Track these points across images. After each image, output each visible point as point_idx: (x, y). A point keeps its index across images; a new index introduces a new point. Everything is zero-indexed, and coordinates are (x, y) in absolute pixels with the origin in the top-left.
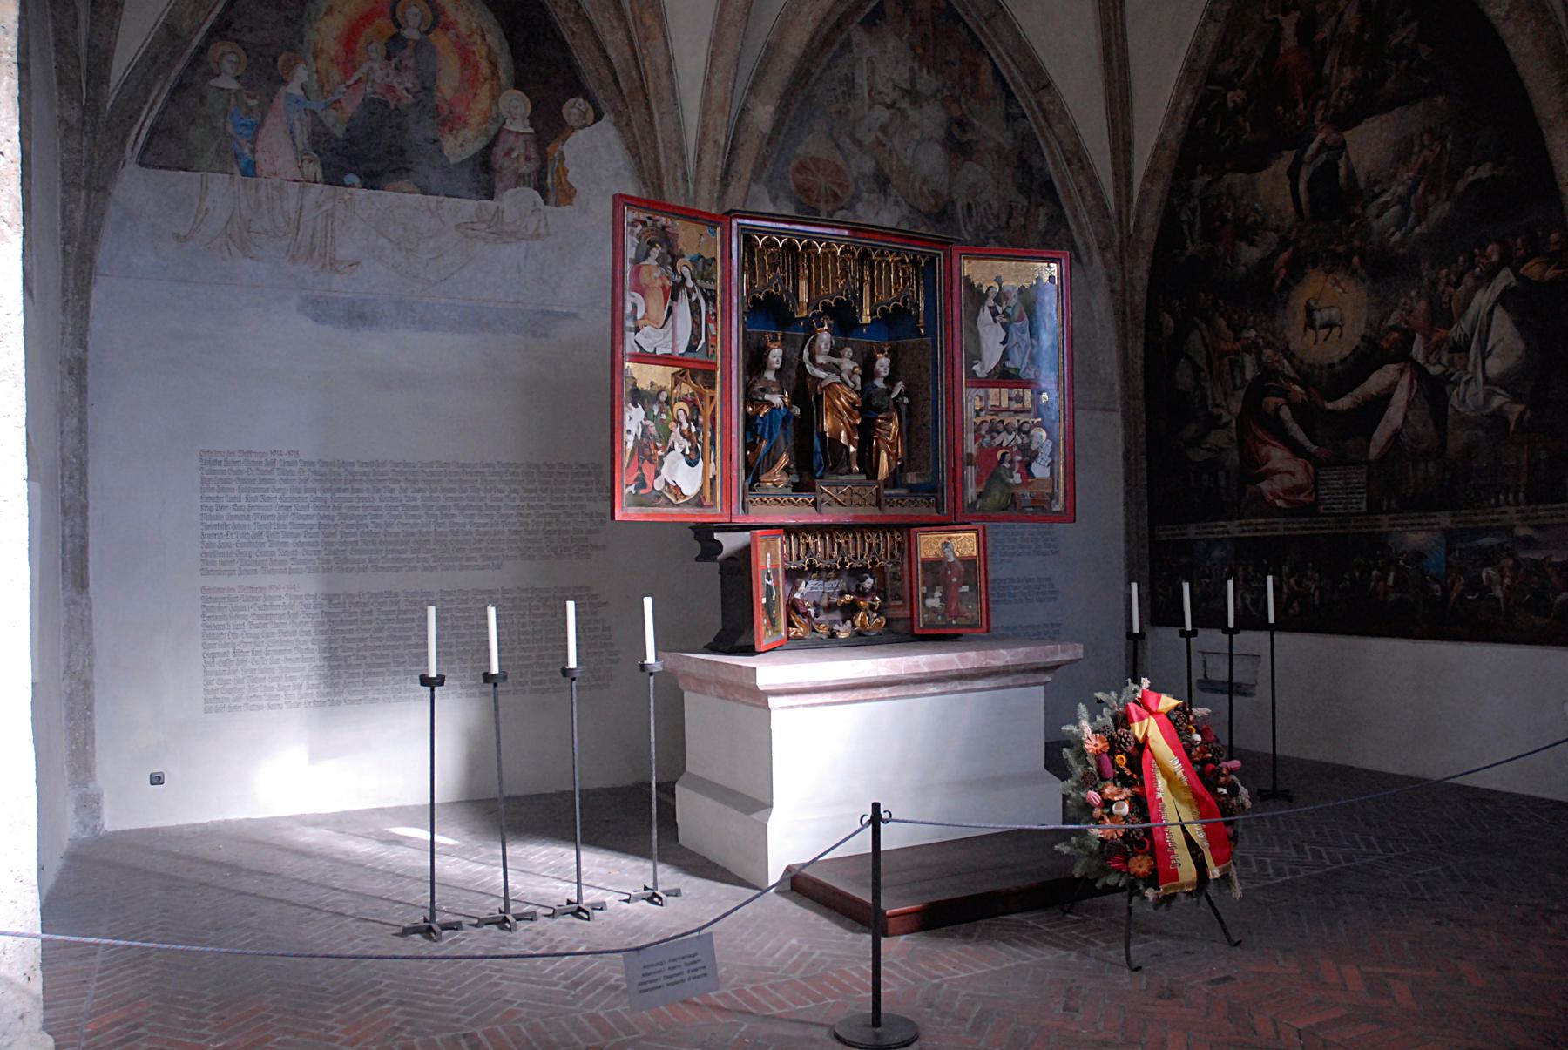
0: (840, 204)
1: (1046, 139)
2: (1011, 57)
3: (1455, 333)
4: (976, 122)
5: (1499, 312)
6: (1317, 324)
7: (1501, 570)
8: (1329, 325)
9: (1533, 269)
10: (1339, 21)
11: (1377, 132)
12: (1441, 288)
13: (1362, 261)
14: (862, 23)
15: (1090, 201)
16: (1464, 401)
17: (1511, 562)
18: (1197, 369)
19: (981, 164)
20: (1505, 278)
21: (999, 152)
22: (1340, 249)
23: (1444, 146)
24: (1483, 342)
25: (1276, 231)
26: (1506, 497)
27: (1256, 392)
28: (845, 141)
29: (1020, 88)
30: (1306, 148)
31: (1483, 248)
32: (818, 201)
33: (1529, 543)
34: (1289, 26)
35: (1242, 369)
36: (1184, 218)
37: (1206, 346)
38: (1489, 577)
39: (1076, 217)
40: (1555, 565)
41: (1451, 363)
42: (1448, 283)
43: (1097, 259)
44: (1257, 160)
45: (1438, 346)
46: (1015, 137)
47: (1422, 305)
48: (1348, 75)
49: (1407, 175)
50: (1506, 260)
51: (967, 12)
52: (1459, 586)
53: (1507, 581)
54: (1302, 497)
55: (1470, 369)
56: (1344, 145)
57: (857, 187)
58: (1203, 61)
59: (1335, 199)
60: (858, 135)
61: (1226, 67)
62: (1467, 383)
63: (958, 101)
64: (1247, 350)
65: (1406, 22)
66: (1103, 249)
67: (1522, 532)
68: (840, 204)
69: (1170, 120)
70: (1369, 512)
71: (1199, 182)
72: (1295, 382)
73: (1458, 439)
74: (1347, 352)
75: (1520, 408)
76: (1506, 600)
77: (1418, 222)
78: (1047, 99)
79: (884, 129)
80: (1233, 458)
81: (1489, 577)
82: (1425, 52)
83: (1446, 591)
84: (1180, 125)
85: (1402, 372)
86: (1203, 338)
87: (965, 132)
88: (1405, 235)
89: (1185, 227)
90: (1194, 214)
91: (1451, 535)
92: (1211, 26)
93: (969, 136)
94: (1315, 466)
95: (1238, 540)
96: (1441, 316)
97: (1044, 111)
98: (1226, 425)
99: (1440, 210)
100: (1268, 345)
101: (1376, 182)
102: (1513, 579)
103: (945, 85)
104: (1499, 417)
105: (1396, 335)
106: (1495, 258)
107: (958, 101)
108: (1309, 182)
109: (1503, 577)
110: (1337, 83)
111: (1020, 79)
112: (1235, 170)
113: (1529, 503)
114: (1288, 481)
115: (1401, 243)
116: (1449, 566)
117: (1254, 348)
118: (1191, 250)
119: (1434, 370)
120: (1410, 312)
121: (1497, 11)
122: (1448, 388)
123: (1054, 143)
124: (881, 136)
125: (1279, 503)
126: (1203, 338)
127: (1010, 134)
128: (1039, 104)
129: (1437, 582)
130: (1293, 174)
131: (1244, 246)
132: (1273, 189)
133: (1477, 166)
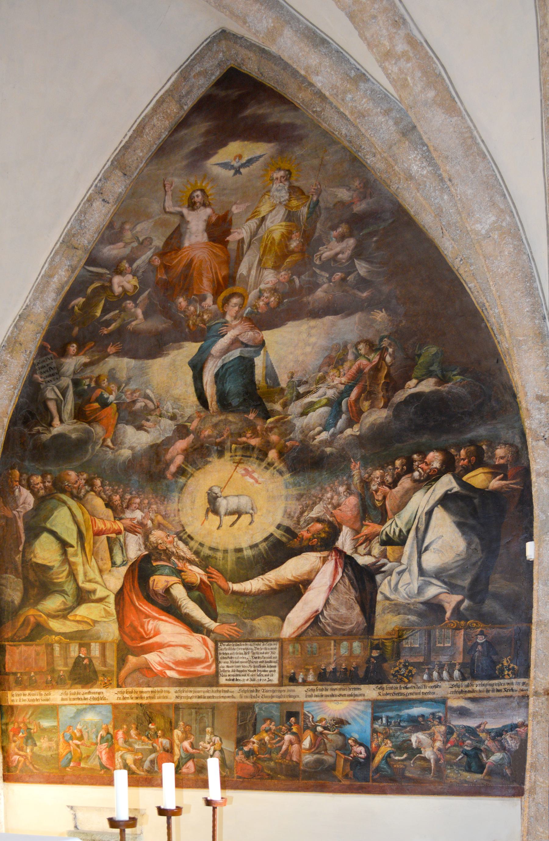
3: (390, 528)
5: (439, 514)
6: (222, 511)
7: (432, 737)
8: (238, 513)
9: (478, 478)
10: (259, 227)
11: (304, 336)
12: (374, 487)
13: (281, 454)
16: (396, 589)
17: (443, 728)
18: (64, 545)
20: (447, 483)
22: (254, 442)
23: (382, 358)
24: (420, 541)
25: (173, 418)
26: (440, 674)
27: (141, 572)
30: (215, 342)
31: (423, 454)
33: (463, 712)
34: (197, 223)
35: (124, 548)
36: (50, 394)
37: (76, 522)
38: (419, 742)
40: (489, 732)
41: (384, 555)
42: (383, 483)
44: (155, 346)
45: (369, 539)
47: (353, 500)
48: (270, 277)
49: (338, 380)
50: (449, 466)
52: (386, 748)
53: (438, 744)
54: (199, 669)
55: (404, 560)
56: (262, 344)
58: (87, 240)
59: (246, 394)
61: (111, 251)
62: (400, 573)
64: (131, 530)
65: (342, 238)
67: (455, 703)
69: (40, 290)
70: (281, 684)
71: (71, 363)
72: (191, 562)
73: (386, 624)
74: (258, 538)
75: (459, 598)
76: (437, 761)
77: (350, 424)
80: (110, 631)
81: (419, 742)
82: (362, 268)
83: (371, 756)
84: (51, 301)
85: (325, 560)
86: (73, 516)
88: (334, 435)
89: (52, 406)
90: (64, 392)
91: (377, 706)
92: (97, 204)
94: (216, 642)
95: (115, 706)
96: (372, 510)
98: (101, 600)
99: (376, 416)
100: (159, 526)
101: (301, 383)
102: (445, 742)
104: (434, 608)
105: (319, 526)
106: (436, 465)
108: (217, 376)
109: (434, 741)
110: (257, 284)
112: (118, 354)
113: (464, 679)
114: (181, 654)
115: (329, 443)
116: (374, 731)
117: (141, 529)
118: (58, 428)
119: (363, 560)
120: (337, 506)
121: (478, 227)
122: (378, 578)
125: (170, 673)
126: (73, 516)
129: (361, 745)
130: (197, 367)
131: (130, 430)
132: (170, 378)
133: (420, 381)
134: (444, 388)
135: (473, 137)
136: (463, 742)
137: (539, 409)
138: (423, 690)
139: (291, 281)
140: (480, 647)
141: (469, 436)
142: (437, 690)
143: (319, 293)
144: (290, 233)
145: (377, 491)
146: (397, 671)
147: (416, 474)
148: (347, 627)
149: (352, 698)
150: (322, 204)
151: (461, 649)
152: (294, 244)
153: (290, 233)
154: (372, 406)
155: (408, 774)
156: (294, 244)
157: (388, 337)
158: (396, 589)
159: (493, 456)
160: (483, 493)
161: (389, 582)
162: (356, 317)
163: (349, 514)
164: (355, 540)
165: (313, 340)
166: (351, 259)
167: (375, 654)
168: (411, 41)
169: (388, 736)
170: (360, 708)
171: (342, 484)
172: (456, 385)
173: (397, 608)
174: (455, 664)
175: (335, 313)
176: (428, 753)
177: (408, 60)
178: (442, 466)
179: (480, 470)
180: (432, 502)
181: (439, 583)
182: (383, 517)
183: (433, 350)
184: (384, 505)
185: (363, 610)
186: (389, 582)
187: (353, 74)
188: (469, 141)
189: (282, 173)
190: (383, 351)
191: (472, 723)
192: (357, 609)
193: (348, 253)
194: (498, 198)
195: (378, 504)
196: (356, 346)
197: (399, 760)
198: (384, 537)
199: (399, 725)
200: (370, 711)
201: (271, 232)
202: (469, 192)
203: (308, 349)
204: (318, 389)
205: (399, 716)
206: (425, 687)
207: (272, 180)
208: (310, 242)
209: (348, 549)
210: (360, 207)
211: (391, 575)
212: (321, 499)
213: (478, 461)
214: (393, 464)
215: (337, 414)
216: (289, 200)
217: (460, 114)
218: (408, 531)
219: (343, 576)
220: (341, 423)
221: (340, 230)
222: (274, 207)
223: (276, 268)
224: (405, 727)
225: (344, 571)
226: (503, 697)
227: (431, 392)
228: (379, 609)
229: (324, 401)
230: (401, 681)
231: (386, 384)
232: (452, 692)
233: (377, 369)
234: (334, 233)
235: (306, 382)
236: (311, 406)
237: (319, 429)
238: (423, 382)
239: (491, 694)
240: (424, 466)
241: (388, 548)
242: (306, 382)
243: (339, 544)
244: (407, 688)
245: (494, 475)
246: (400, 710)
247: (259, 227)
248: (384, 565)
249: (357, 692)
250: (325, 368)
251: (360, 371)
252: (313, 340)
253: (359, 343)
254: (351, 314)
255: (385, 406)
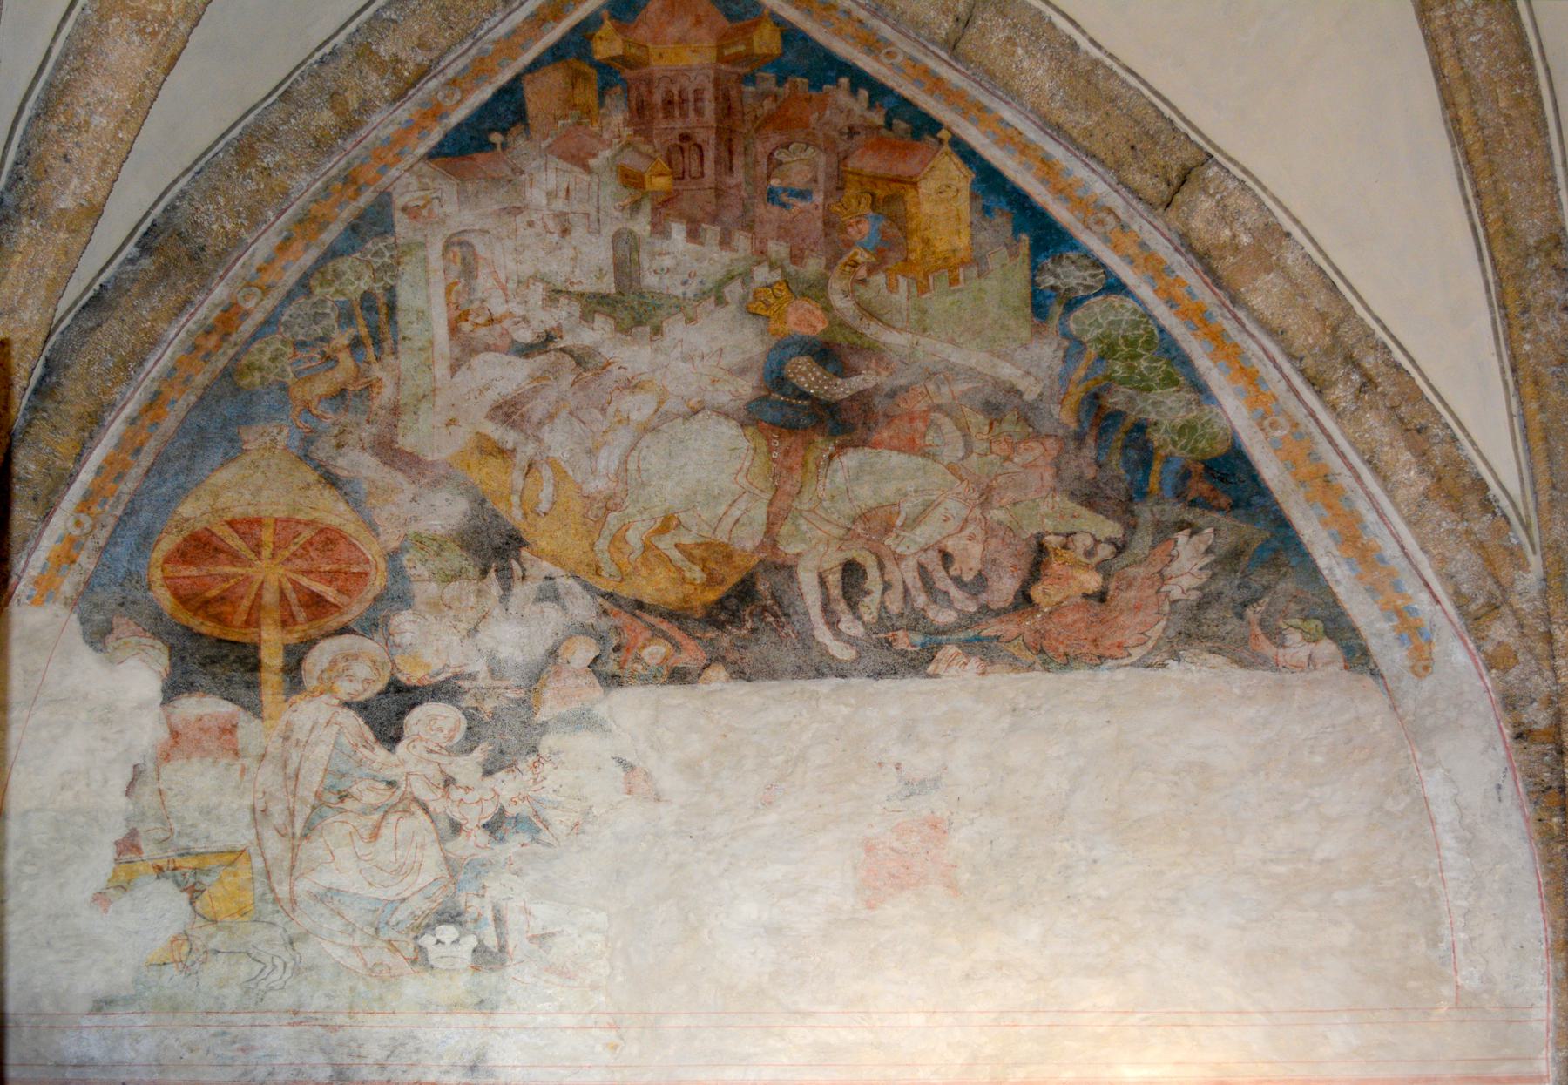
0: (334, 622)
1: (1217, 338)
2: (1056, 130)
4: (895, 339)
14: (431, 156)
15: (1412, 479)
19: (911, 447)
21: (999, 406)
28: (359, 464)
29: (1093, 211)
32: (252, 622)
39: (1351, 538)
43: (1456, 655)
46: (1074, 346)
51: (873, 45)
57: (397, 572)
60: (406, 442)
63: (816, 290)
66: (1474, 620)
68: (334, 622)
78: (1200, 212)
79: (508, 411)
87: (845, 371)
93: (856, 383)
97: (1204, 259)
103: (761, 255)
107: (816, 290)
111: (1100, 188)
123: (1256, 347)
124: (494, 431)
127: (1047, 352)
128: (1186, 244)
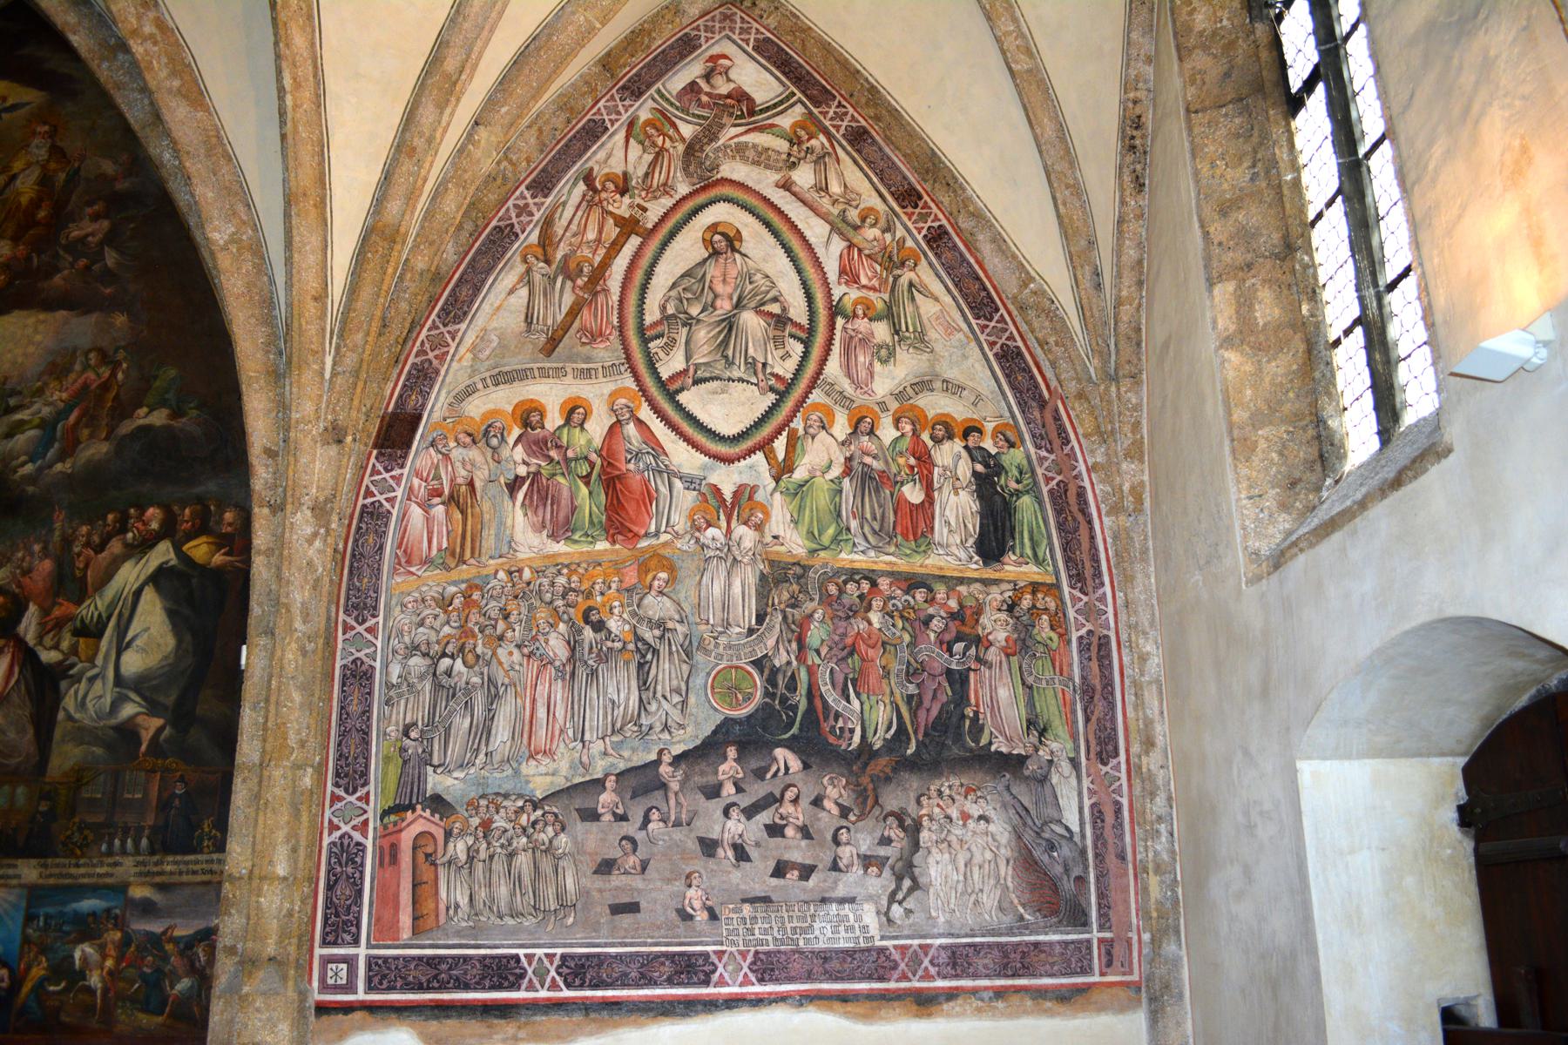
3: (89, 610)
5: (149, 595)
7: (102, 949)
9: (199, 549)
11: (29, 331)
20: (164, 553)
23: (113, 375)
24: (122, 630)
26: (123, 843)
31: (142, 509)
33: (147, 909)
38: (84, 959)
41: (74, 650)
42: (88, 544)
47: (47, 565)
50: (169, 530)
55: (99, 661)
62: (92, 680)
65: (95, 218)
67: (138, 892)
73: (65, 757)
76: (105, 991)
77: (61, 458)
82: (111, 258)
88: (40, 470)
99: (95, 450)
101: (14, 393)
102: (118, 960)
104: (128, 732)
106: (154, 525)
109: (104, 957)
113: (152, 853)
115: (32, 479)
116: (26, 940)
119: (48, 656)
122: (63, 684)
134: (179, 424)
135: (218, 137)
136: (143, 959)
137: (267, 466)
138: (99, 870)
139: (28, 259)
140: (177, 802)
141: (198, 490)
142: (119, 869)
143: (57, 279)
144: (41, 200)
145: (79, 555)
146: (69, 837)
147: (130, 535)
148: (14, 761)
149: (1023, 813)
150: (82, 173)
151: (154, 803)
152: (42, 214)
153: (41, 200)
154: (91, 436)
155: (65, 1018)
156: (42, 214)
157: (124, 348)
158: (82, 705)
159: (220, 521)
160: (203, 570)
161: (76, 693)
162: (93, 318)
163: (41, 584)
164: (41, 624)
165: (38, 338)
166: (101, 244)
167: (43, 807)
168: (160, 24)
169: (44, 950)
170: (12, 898)
171: (37, 541)
172: (189, 423)
173: (82, 734)
174: (143, 828)
175: (70, 308)
176: (95, 980)
177: (155, 43)
178: (161, 526)
179: (203, 539)
180: (142, 578)
181: (138, 699)
182: (81, 595)
183: (172, 373)
184: (85, 575)
185: (37, 733)
186: (76, 693)
187: (113, 41)
188: (214, 140)
189: (46, 128)
190: (116, 365)
191: (156, 927)
192: (31, 732)
193: (99, 236)
194: (240, 208)
195: (78, 574)
196: (86, 354)
197: (54, 993)
198: (78, 624)
199: (60, 930)
200: (24, 904)
201: (19, 194)
202: (210, 194)
203: (31, 349)
204: (32, 403)
205: (62, 914)
206: (102, 864)
207: (34, 134)
208: (61, 216)
209: (30, 638)
210: (122, 185)
211: (79, 681)
212: (9, 560)
213: (201, 529)
214: (105, 518)
215: (47, 442)
216: (48, 161)
217: (208, 110)
218: (109, 618)
219: (18, 681)
220: (51, 454)
221: (96, 207)
222: (29, 165)
223: (15, 239)
224: (68, 933)
225: (20, 672)
226: (198, 884)
227: (163, 426)
228: (58, 734)
229: (36, 421)
230: (72, 854)
231: (113, 409)
232: (140, 874)
233: (105, 387)
234: (89, 210)
235: (20, 393)
236: (19, 427)
237: (23, 458)
238: (155, 413)
239: (185, 878)
240: (139, 525)
241: (81, 640)
242: (20, 393)
243: (21, 628)
244: (77, 866)
245: (219, 547)
246: (64, 903)
247: (7, 184)
248: (73, 666)
249: (11, 872)
250: (45, 378)
251: (85, 386)
252: (38, 338)
253: (90, 351)
254: (87, 312)
255: (107, 439)
